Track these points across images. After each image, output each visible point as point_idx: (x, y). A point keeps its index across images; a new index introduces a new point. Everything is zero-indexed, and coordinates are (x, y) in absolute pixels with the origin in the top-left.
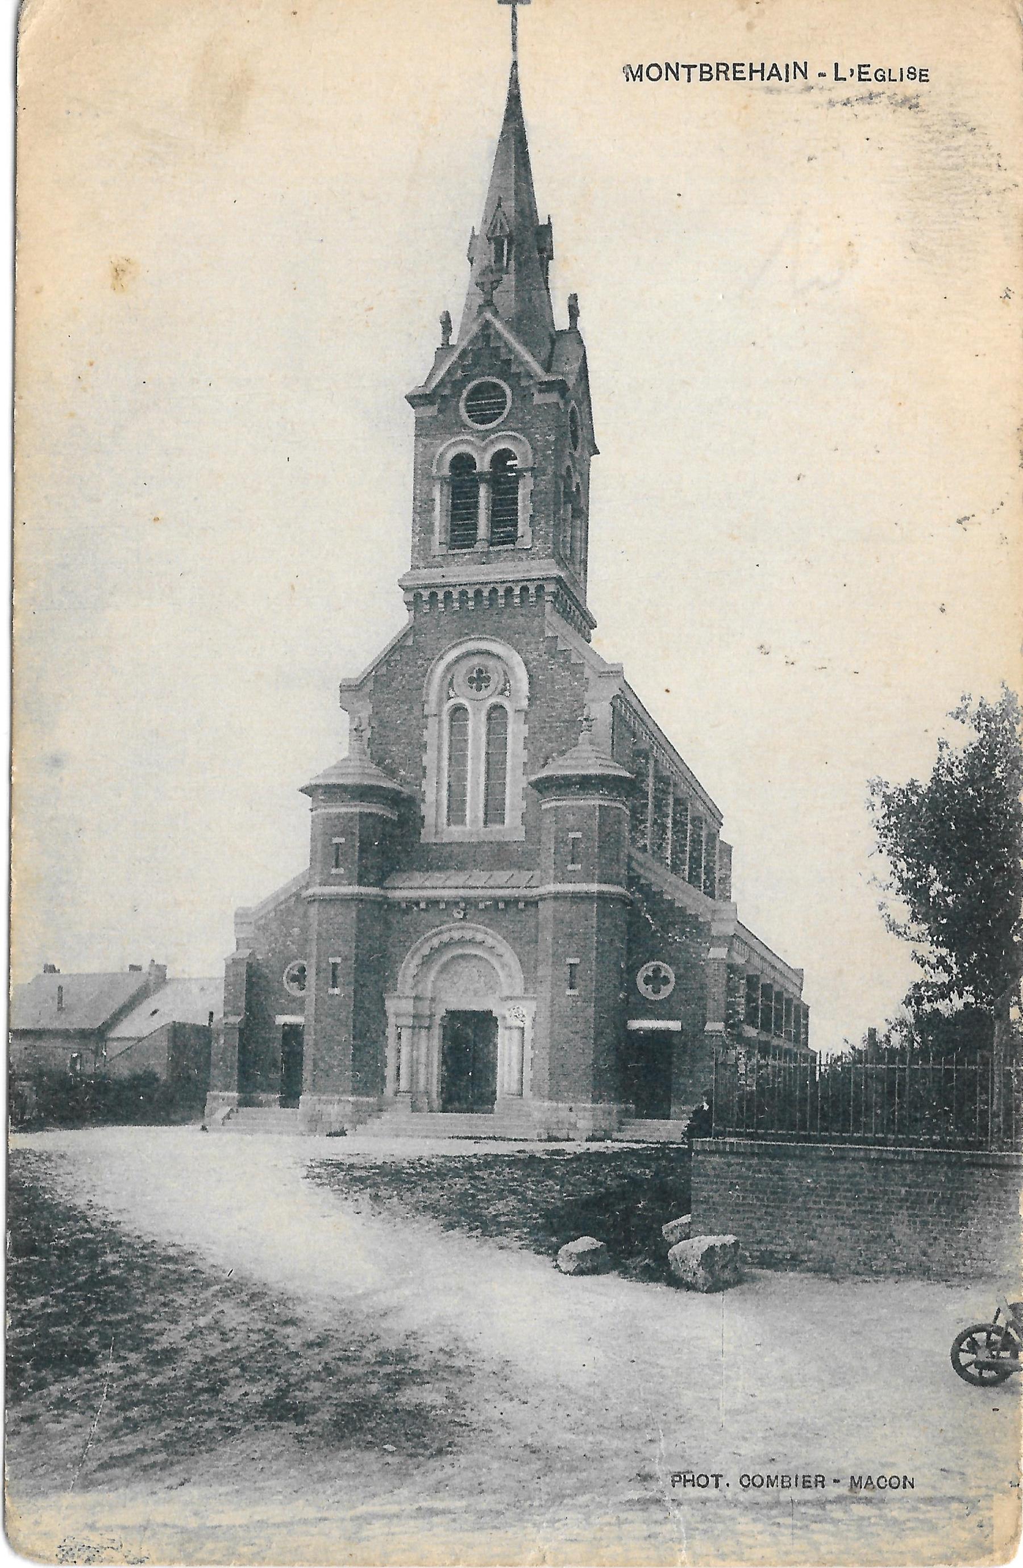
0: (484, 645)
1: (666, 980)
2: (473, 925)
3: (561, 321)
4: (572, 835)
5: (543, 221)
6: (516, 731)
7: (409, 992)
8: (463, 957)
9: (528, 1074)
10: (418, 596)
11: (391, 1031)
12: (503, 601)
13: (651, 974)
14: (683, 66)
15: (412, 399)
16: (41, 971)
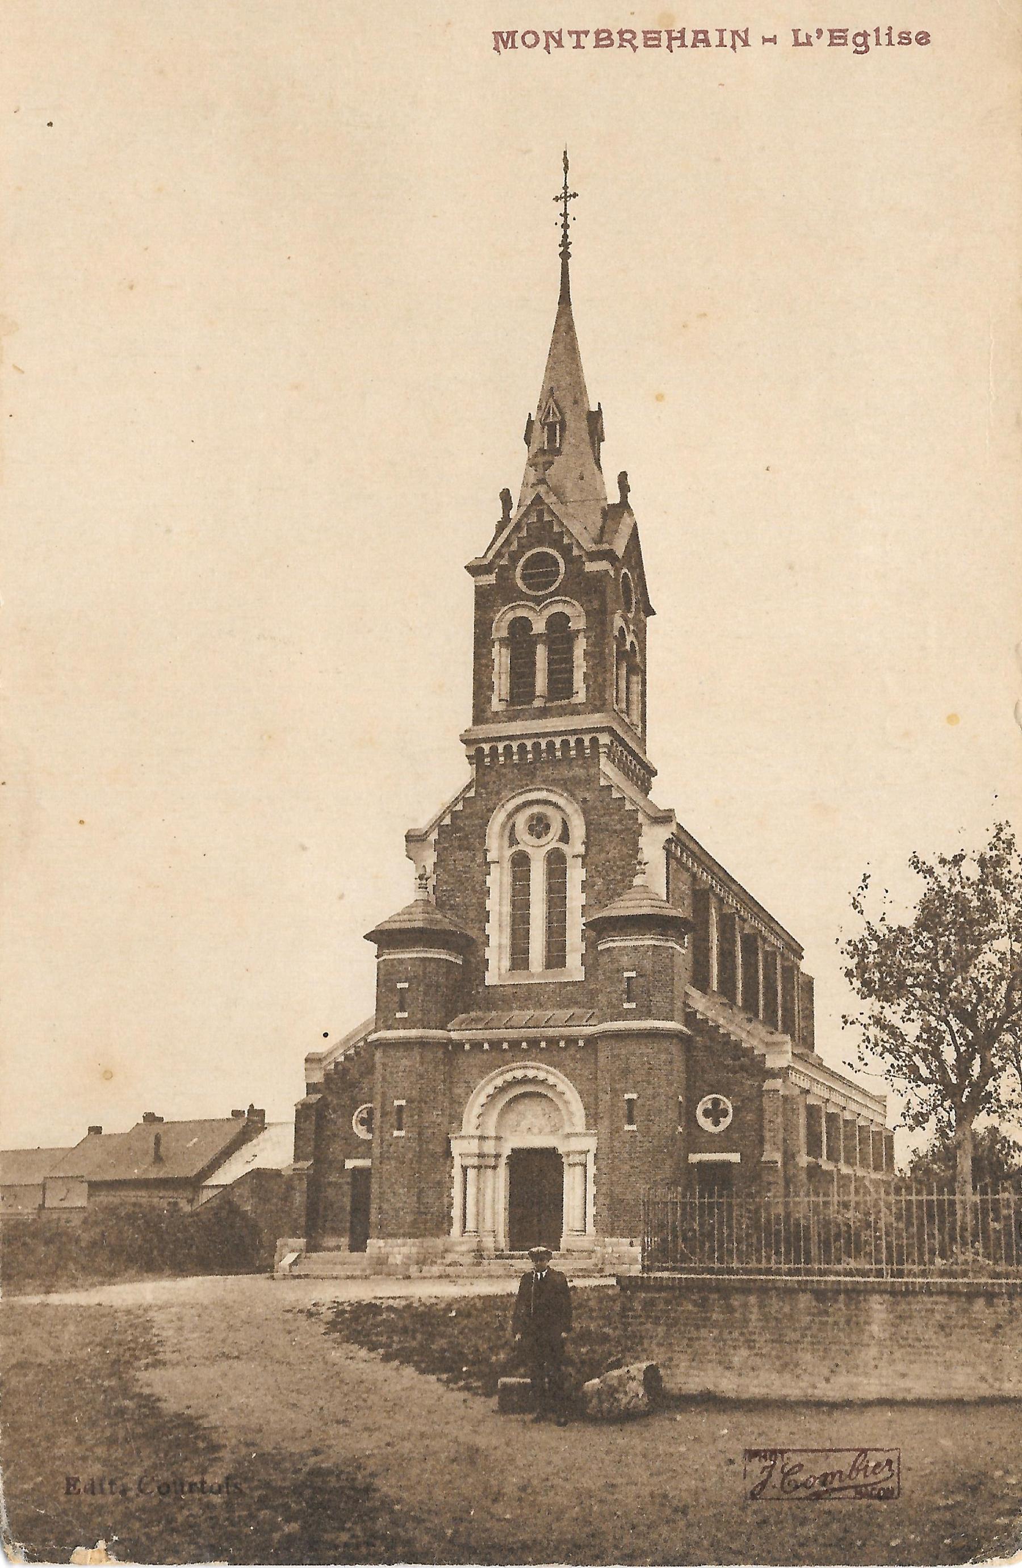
0: (553, 798)
1: (725, 1113)
2: (534, 1064)
4: (626, 974)
5: (594, 408)
6: (576, 875)
7: (473, 1132)
8: (540, 1095)
9: (591, 1211)
10: (480, 750)
11: (457, 1172)
13: (366, 1116)
14: (570, 33)
15: (474, 570)
16: (141, 1121)
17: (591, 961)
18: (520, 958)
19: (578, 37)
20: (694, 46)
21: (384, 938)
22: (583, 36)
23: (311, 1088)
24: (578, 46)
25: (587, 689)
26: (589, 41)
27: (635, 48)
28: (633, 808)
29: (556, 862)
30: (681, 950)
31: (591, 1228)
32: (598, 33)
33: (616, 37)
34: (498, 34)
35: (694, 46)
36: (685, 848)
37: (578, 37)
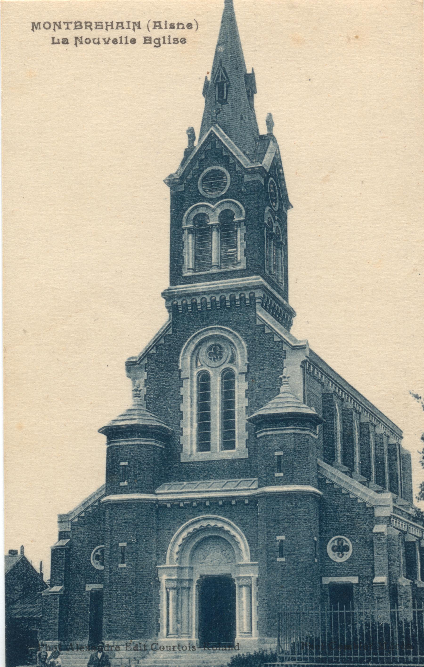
1: (346, 549)
3: (263, 130)
4: (276, 454)
5: (249, 71)
6: (241, 387)
8: (219, 537)
12: (239, 303)
14: (64, 23)
17: (252, 444)
18: (204, 443)
19: (68, 25)
20: (117, 28)
21: (112, 432)
22: (69, 24)
23: (62, 535)
24: (68, 28)
25: (247, 260)
26: (72, 26)
27: (91, 29)
28: (279, 340)
29: (228, 378)
30: (315, 434)
31: (254, 630)
32: (76, 23)
33: (83, 25)
34: (33, 23)
35: (117, 28)
36: (316, 366)
37: (68, 25)
